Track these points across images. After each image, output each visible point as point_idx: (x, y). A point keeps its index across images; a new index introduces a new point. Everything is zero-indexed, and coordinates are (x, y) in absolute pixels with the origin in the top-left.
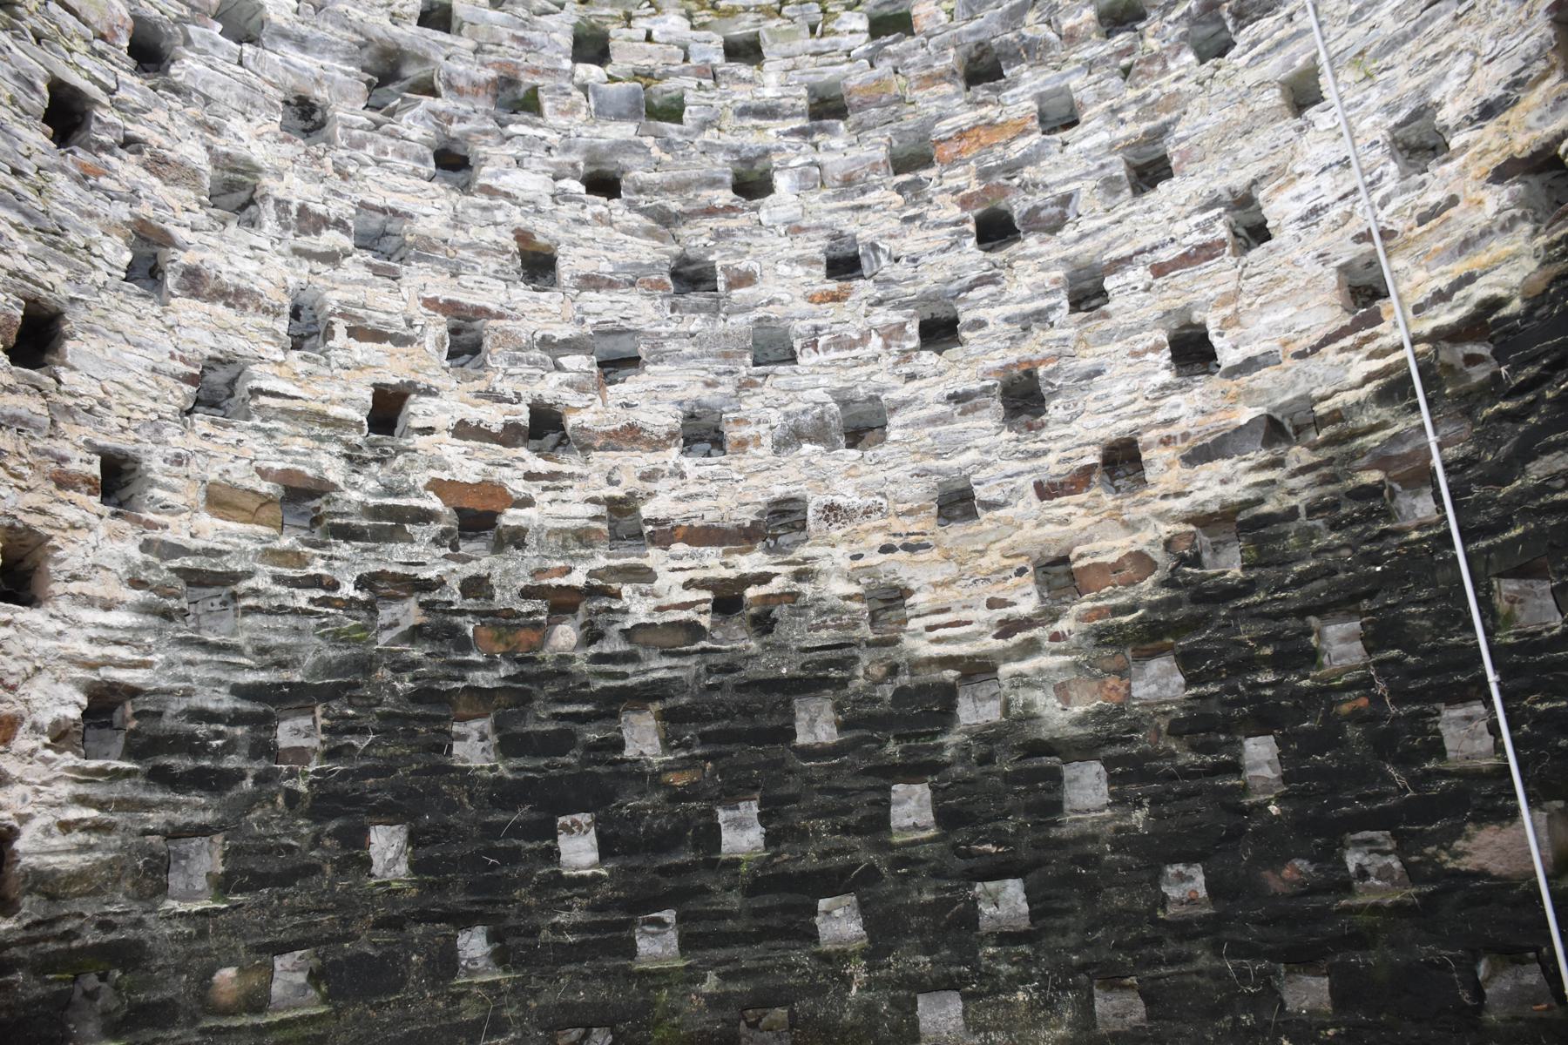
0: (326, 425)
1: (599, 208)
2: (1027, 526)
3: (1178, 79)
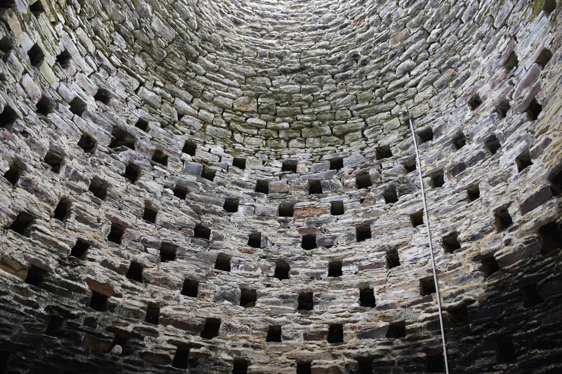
0: (56, 247)
1: (176, 201)
2: (298, 349)
3: (378, 207)
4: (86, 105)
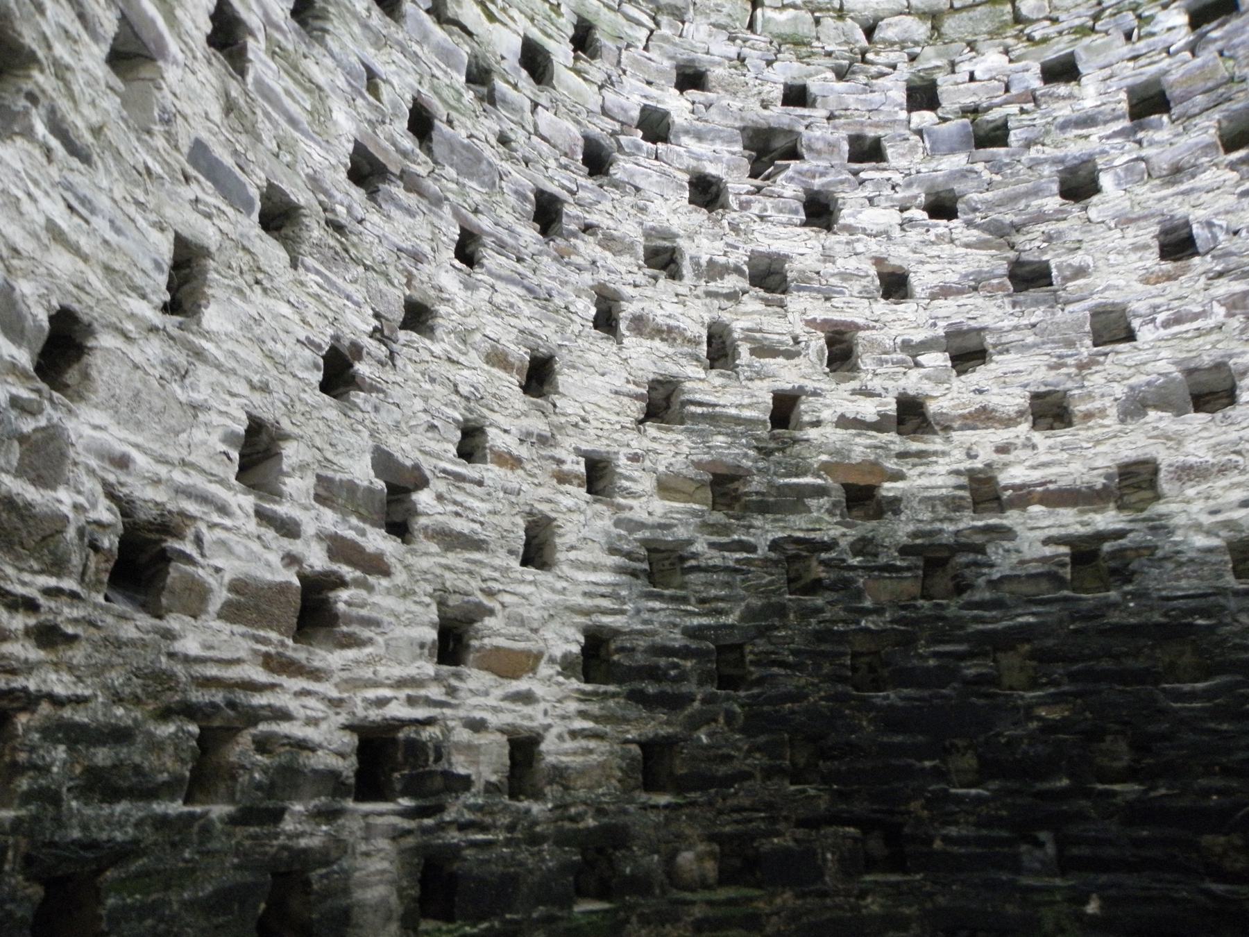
1: (941, 230)
4: (666, 114)
